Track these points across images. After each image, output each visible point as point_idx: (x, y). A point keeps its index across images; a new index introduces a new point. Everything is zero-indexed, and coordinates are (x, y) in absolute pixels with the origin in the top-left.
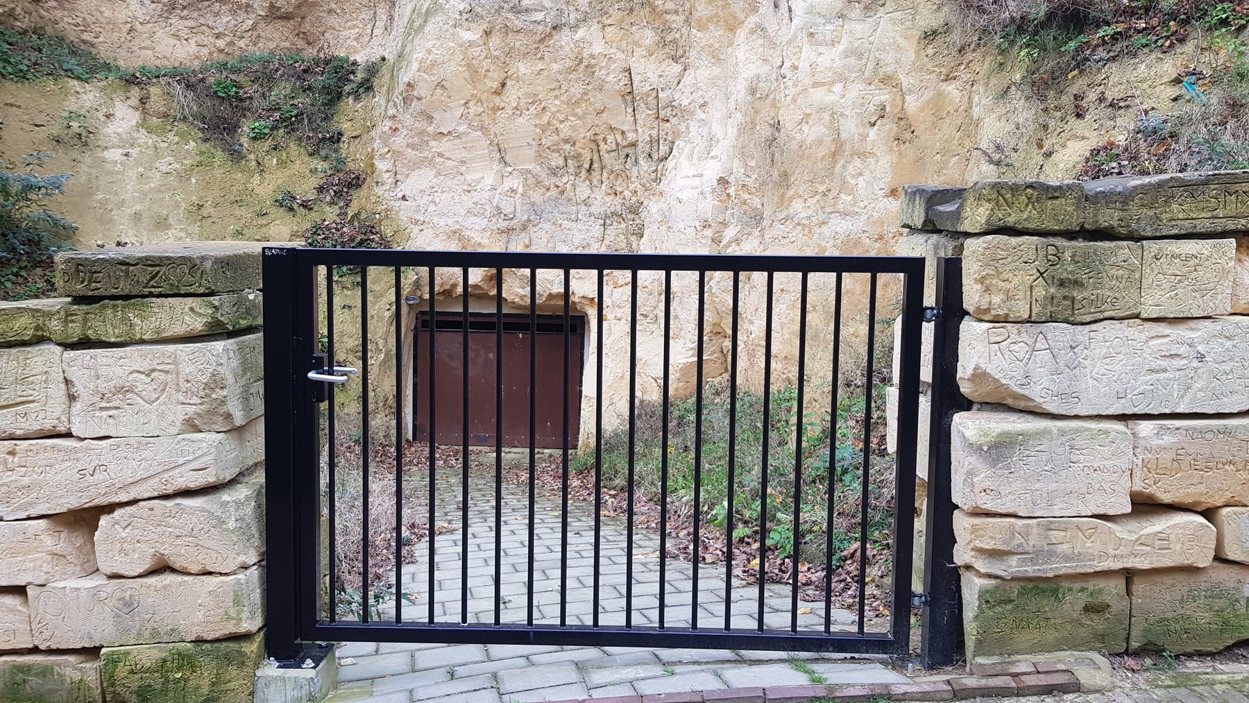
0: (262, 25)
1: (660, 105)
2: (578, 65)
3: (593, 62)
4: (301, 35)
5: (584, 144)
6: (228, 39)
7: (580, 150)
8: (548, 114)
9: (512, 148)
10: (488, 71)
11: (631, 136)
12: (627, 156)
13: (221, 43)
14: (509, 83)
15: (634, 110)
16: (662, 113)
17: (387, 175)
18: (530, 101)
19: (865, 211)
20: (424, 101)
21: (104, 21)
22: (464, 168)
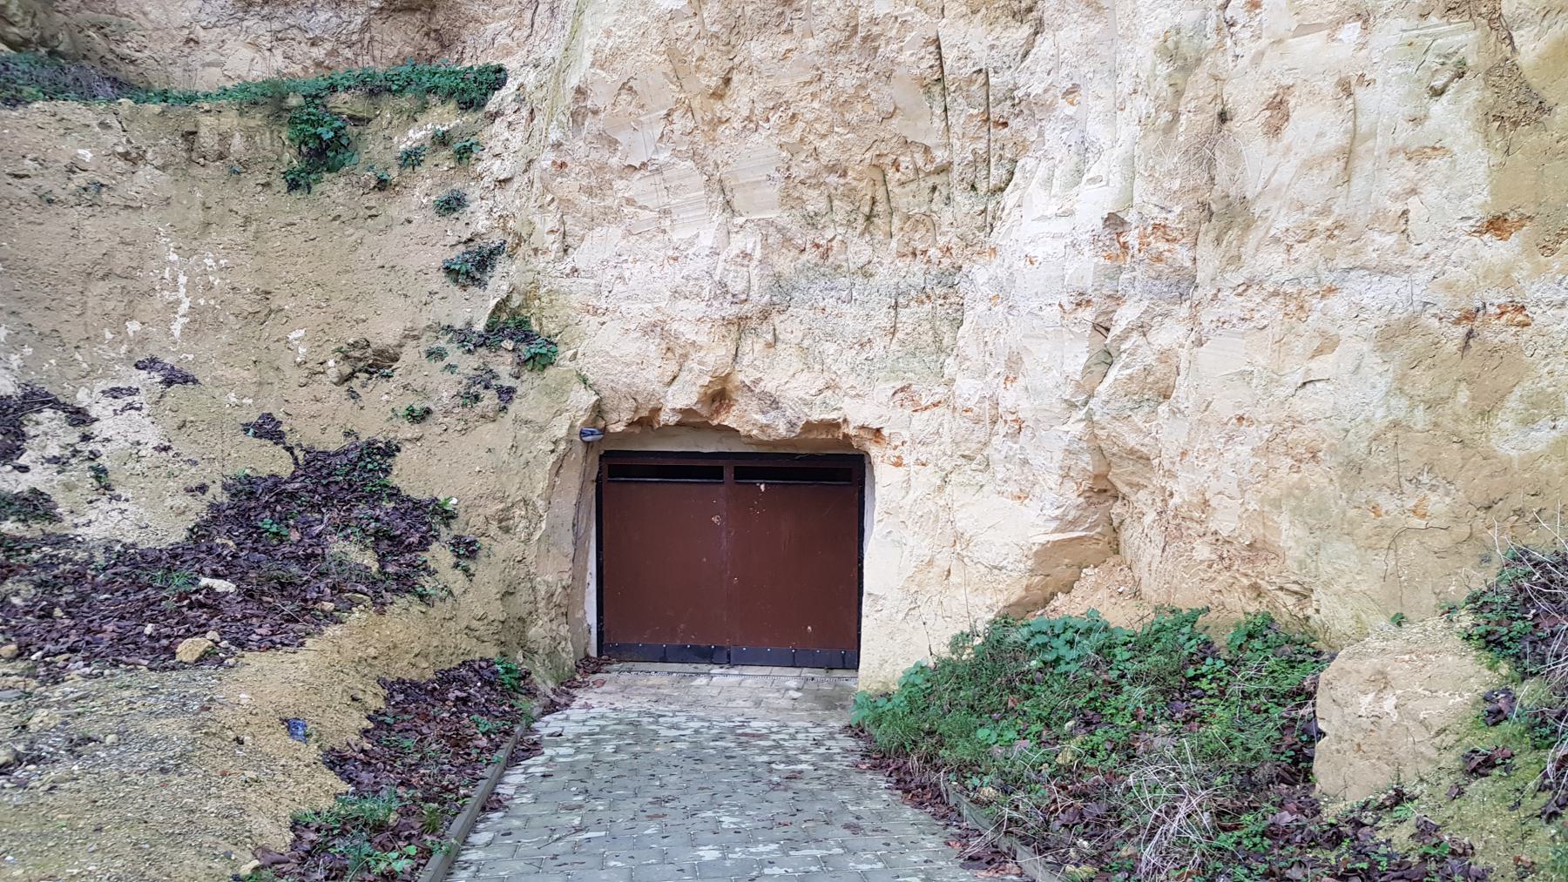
0: (377, 24)
1: (991, 98)
2: (850, 37)
3: (876, 30)
4: (432, 35)
5: (861, 172)
6: (328, 46)
7: (855, 183)
8: (800, 125)
9: (743, 185)
10: (701, 59)
11: (940, 156)
12: (934, 189)
13: (318, 53)
14: (736, 77)
15: (946, 110)
16: (995, 112)
17: (552, 237)
18: (771, 104)
19: (1427, 264)
20: (602, 115)
21: (149, 26)
22: (668, 222)
